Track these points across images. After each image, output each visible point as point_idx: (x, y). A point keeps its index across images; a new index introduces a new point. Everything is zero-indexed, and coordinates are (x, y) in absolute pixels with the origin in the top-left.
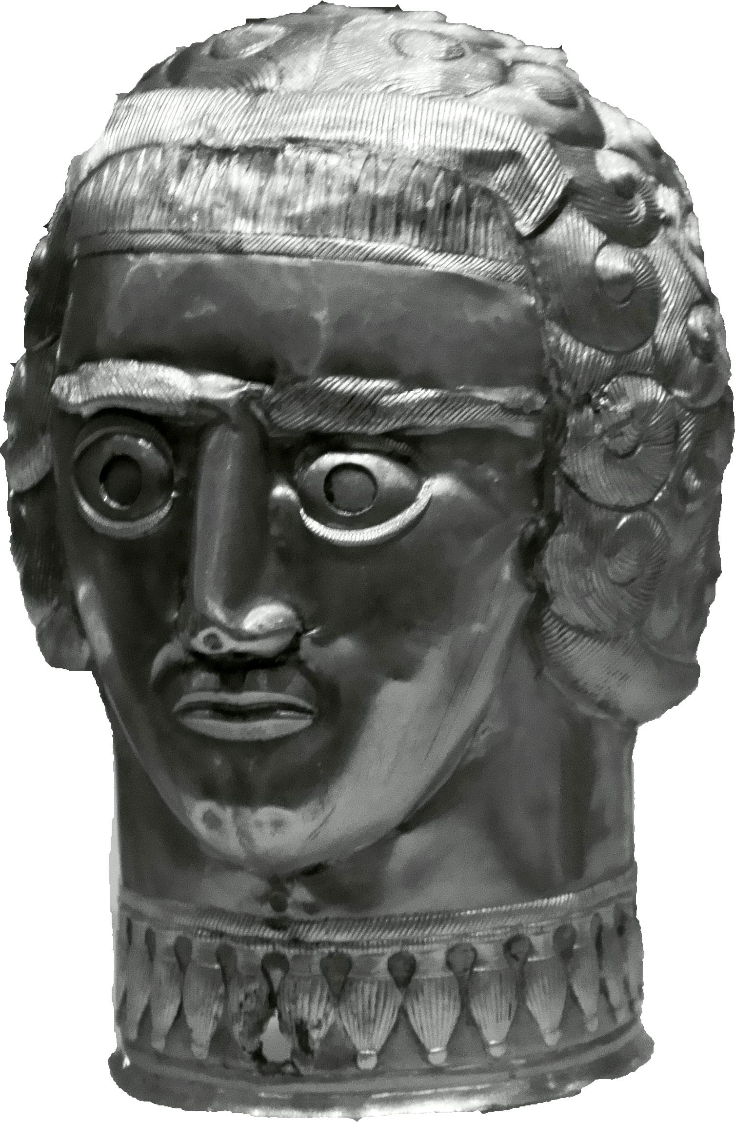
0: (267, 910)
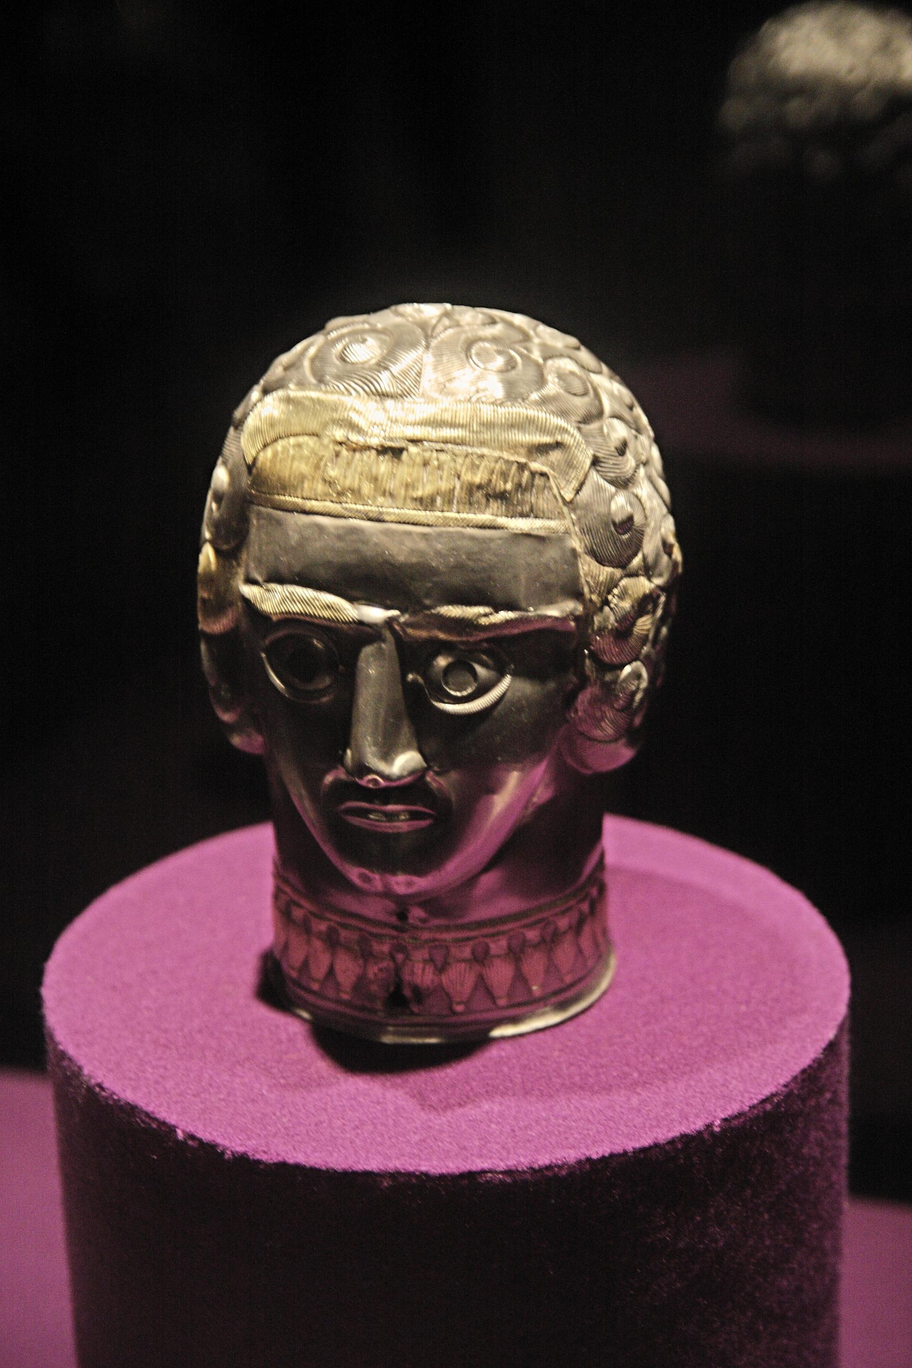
0: (394, 920)
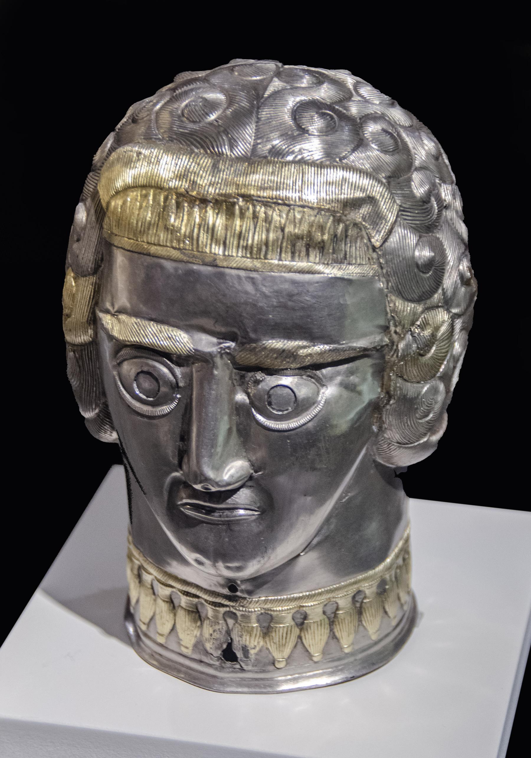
0: (226, 591)
